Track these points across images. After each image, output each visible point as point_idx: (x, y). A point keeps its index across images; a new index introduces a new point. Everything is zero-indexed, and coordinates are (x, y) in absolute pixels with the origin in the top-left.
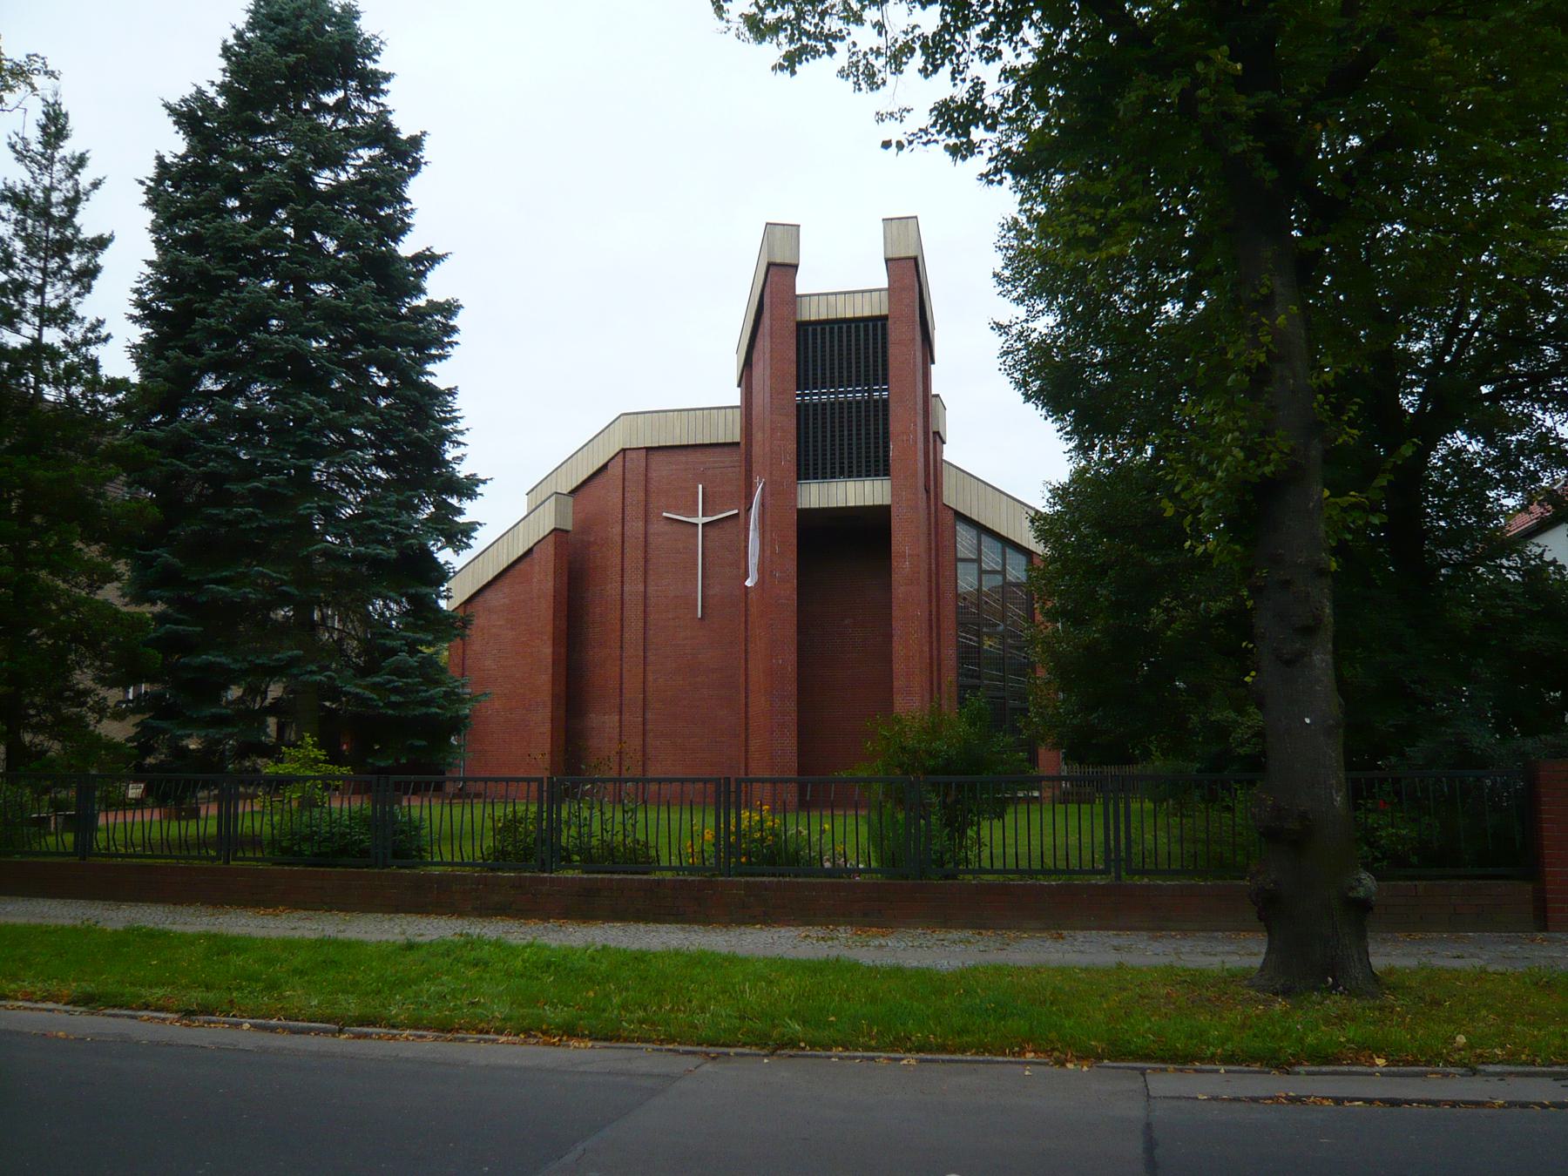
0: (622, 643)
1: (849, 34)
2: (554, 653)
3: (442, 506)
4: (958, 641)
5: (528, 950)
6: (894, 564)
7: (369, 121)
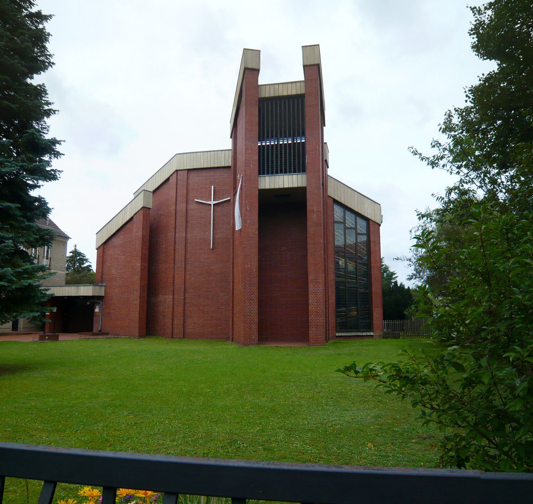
0: (174, 261)
2: (141, 266)
6: (308, 216)
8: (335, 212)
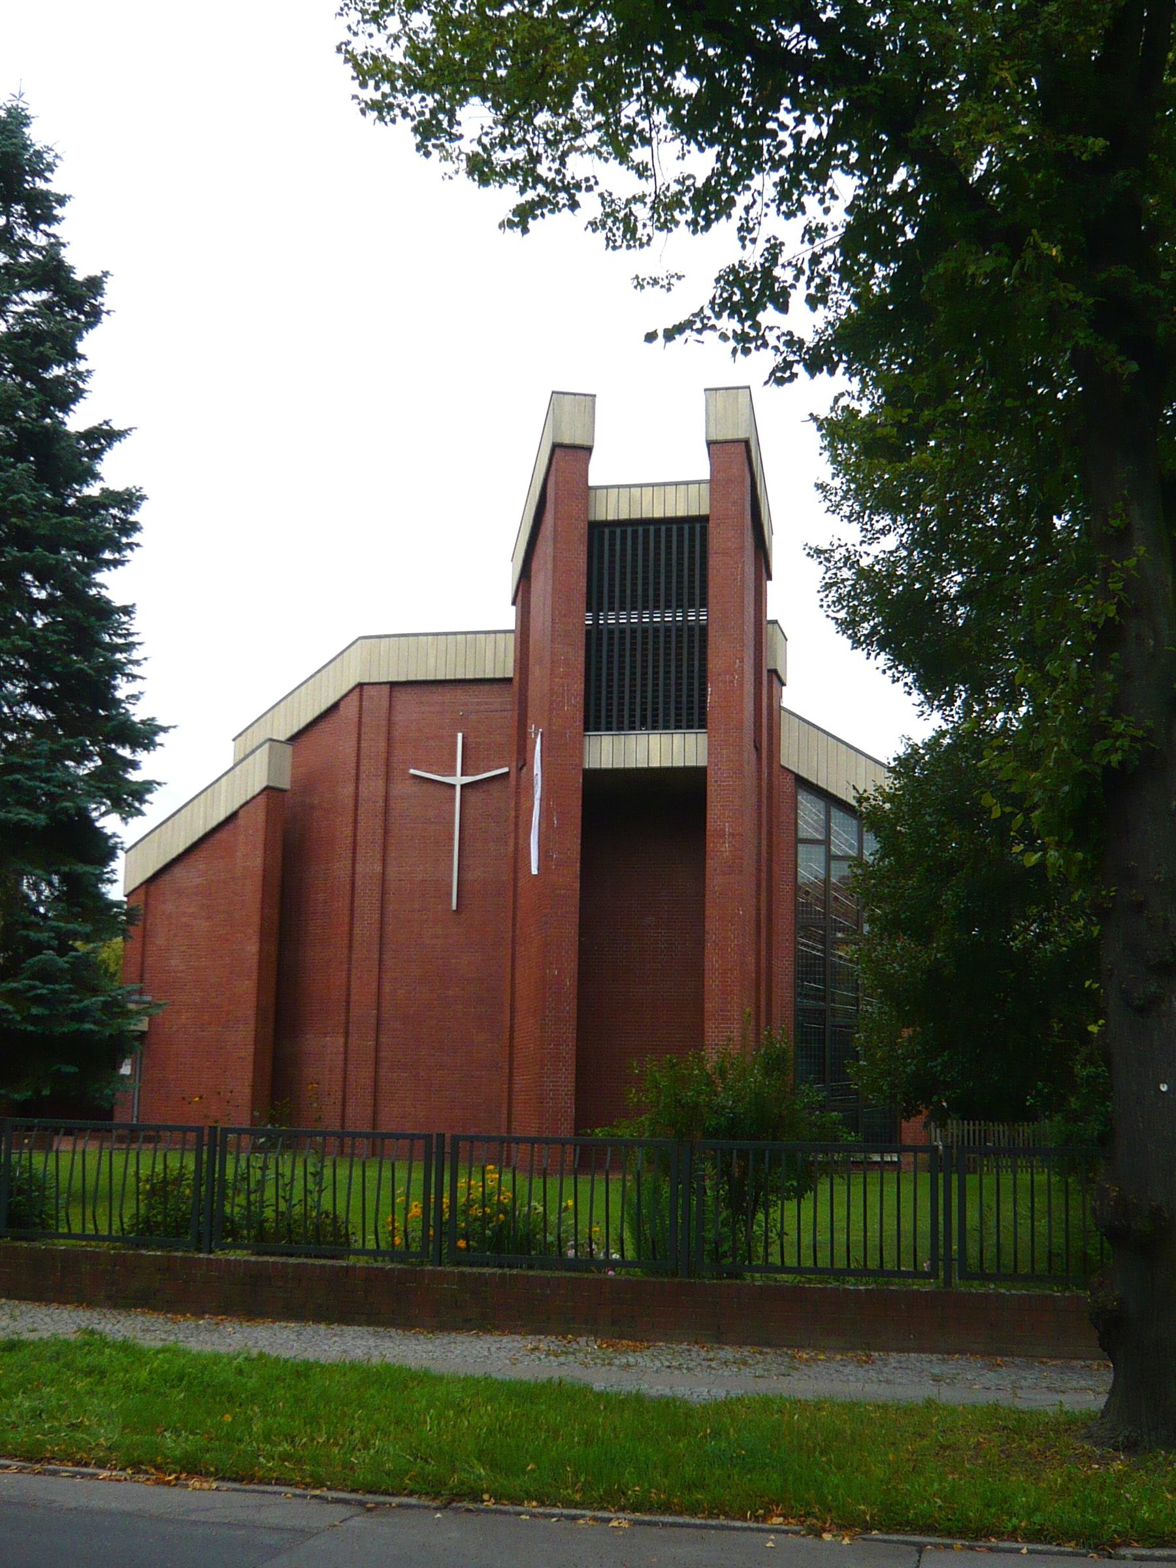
1: (596, 183)
2: (261, 951)
3: (110, 758)
4: (797, 950)
5: (160, 1356)
6: (710, 845)
7: (37, 256)
8: (801, 813)
